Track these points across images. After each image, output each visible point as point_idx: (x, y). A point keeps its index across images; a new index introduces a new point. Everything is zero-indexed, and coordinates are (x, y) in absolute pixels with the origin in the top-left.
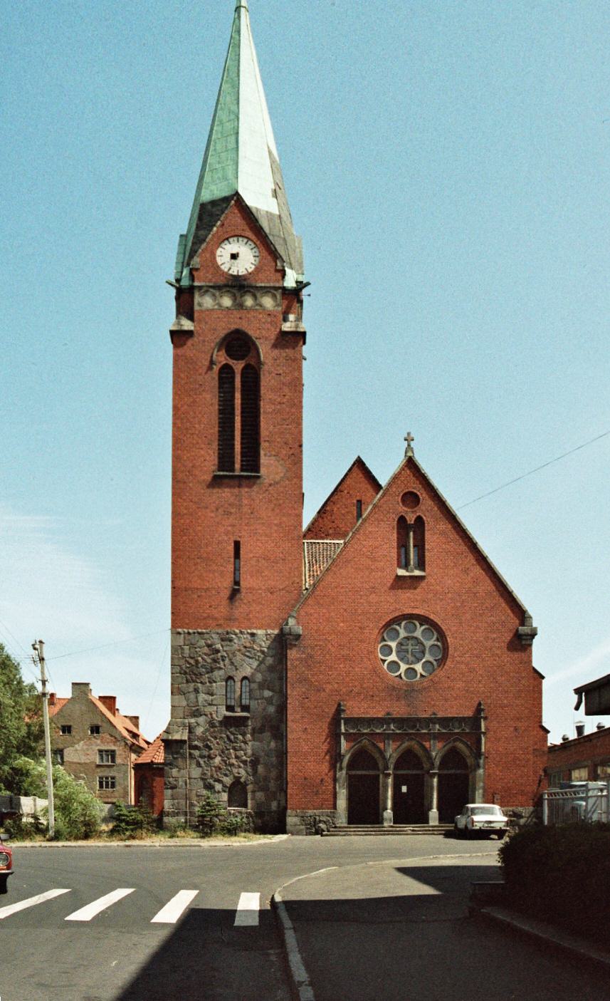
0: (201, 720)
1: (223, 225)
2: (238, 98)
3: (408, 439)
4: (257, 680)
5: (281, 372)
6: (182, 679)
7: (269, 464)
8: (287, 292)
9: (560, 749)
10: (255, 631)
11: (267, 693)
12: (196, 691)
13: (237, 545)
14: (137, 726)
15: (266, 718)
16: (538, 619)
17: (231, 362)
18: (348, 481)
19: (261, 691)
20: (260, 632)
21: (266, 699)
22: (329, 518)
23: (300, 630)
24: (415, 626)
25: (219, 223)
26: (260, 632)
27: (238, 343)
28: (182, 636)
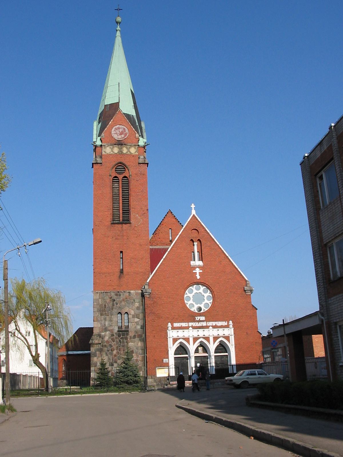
0: (108, 333)
1: (113, 121)
2: (255, 307)
4: (132, 314)
5: (138, 179)
6: (98, 314)
7: (134, 216)
8: (140, 147)
9: (268, 338)
11: (136, 320)
12: (105, 319)
14: (184, 336)
15: (136, 332)
16: (252, 284)
17: (118, 175)
18: (166, 220)
19: (134, 319)
21: (136, 322)
22: (158, 236)
24: (208, 292)
25: (112, 120)
26: (132, 291)
27: (121, 167)
28: (98, 294)
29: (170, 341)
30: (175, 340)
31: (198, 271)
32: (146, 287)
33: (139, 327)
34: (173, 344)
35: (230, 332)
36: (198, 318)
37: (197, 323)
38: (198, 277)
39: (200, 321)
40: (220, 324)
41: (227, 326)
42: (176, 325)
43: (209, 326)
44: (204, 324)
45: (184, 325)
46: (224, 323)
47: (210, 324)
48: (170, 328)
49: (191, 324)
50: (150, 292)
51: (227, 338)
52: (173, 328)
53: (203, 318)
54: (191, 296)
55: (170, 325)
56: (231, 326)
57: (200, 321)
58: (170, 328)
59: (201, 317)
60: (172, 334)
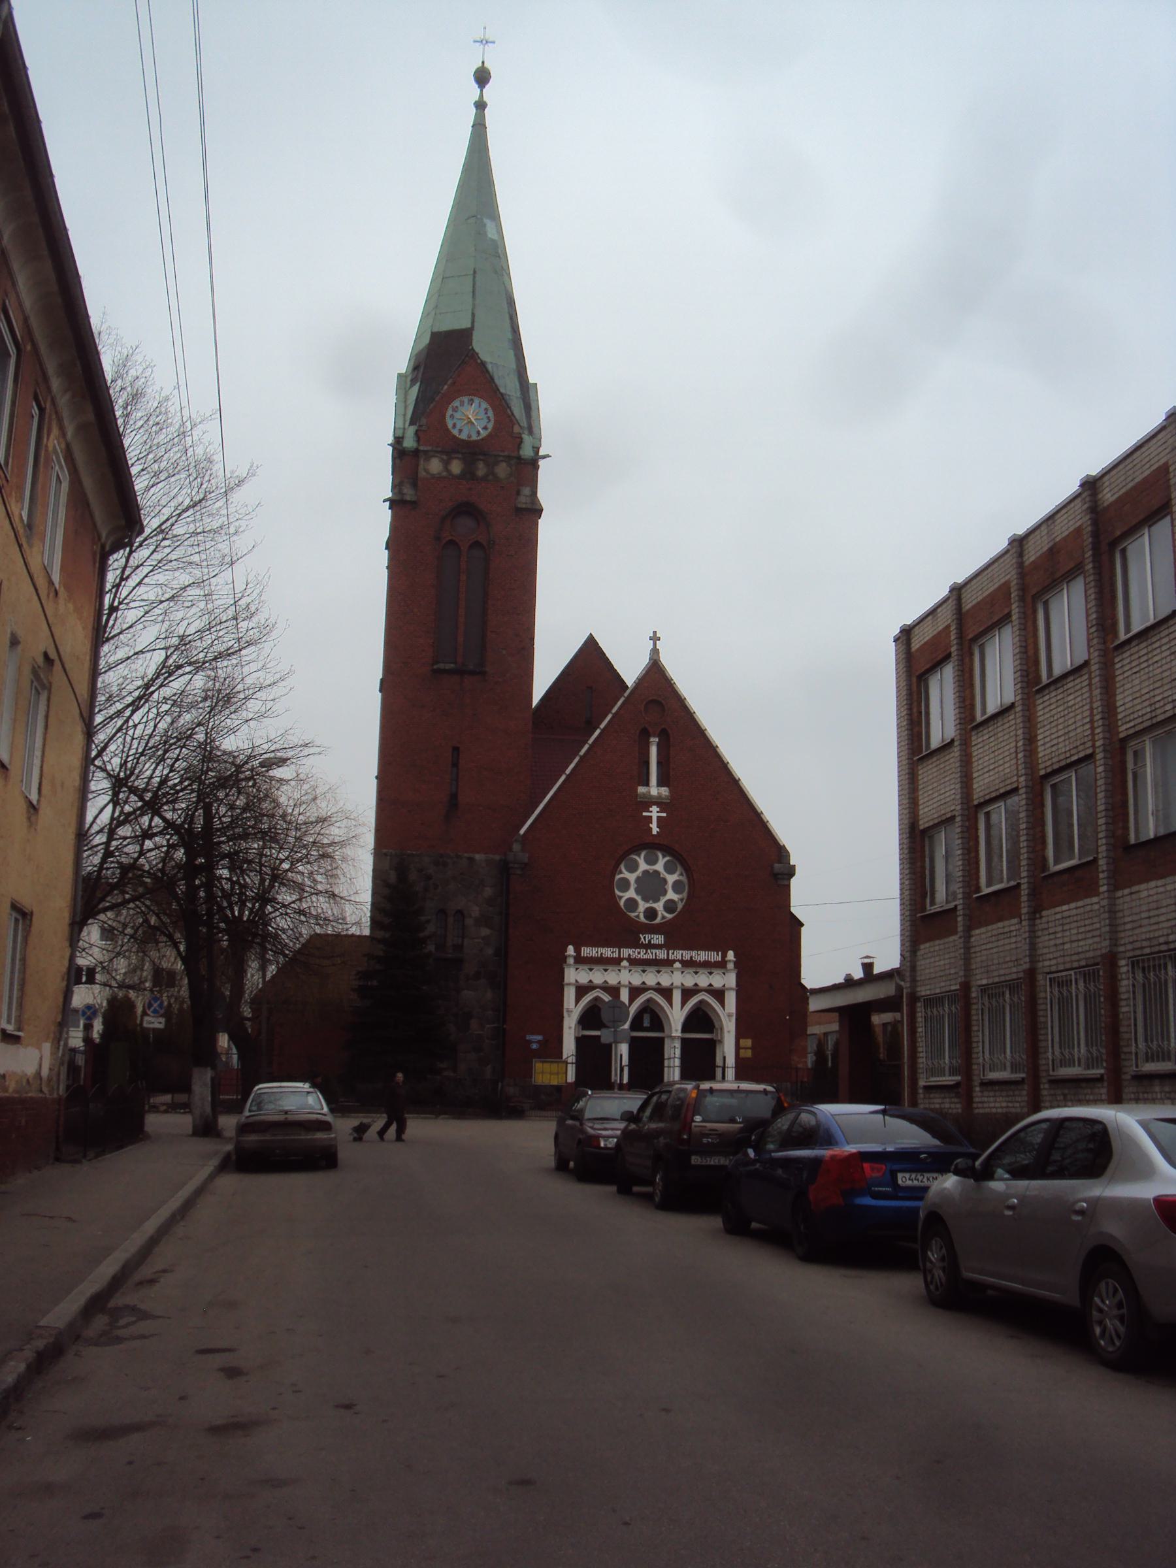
3: (655, 638)
10: (471, 855)
11: (485, 932)
13: (456, 749)
20: (477, 857)
23: (524, 857)
26: (477, 857)
29: (570, 995)
30: (581, 991)
31: (654, 812)
32: (516, 847)
33: (490, 951)
34: (577, 1001)
35: (727, 980)
36: (645, 938)
37: (643, 951)
38: (655, 830)
39: (650, 946)
40: (702, 956)
41: (722, 965)
42: (586, 951)
43: (674, 961)
44: (661, 954)
45: (608, 952)
46: (714, 957)
47: (678, 954)
48: (571, 961)
49: (626, 952)
50: (526, 860)
51: (719, 995)
52: (580, 960)
53: (658, 939)
54: (632, 877)
55: (571, 950)
56: (731, 966)
57: (650, 946)
58: (571, 961)
59: (656, 936)
60: (574, 975)
